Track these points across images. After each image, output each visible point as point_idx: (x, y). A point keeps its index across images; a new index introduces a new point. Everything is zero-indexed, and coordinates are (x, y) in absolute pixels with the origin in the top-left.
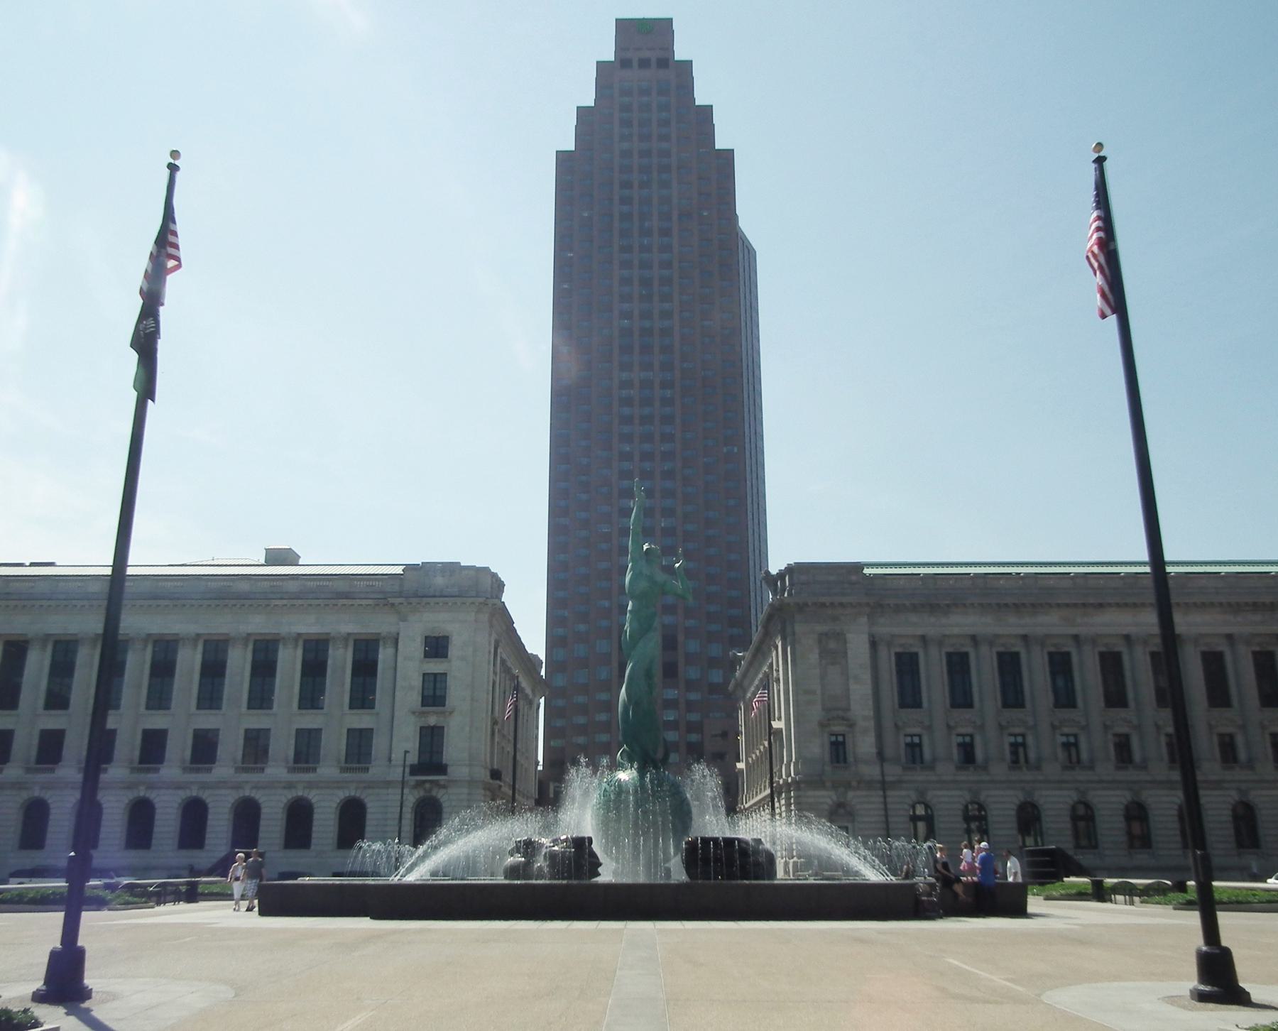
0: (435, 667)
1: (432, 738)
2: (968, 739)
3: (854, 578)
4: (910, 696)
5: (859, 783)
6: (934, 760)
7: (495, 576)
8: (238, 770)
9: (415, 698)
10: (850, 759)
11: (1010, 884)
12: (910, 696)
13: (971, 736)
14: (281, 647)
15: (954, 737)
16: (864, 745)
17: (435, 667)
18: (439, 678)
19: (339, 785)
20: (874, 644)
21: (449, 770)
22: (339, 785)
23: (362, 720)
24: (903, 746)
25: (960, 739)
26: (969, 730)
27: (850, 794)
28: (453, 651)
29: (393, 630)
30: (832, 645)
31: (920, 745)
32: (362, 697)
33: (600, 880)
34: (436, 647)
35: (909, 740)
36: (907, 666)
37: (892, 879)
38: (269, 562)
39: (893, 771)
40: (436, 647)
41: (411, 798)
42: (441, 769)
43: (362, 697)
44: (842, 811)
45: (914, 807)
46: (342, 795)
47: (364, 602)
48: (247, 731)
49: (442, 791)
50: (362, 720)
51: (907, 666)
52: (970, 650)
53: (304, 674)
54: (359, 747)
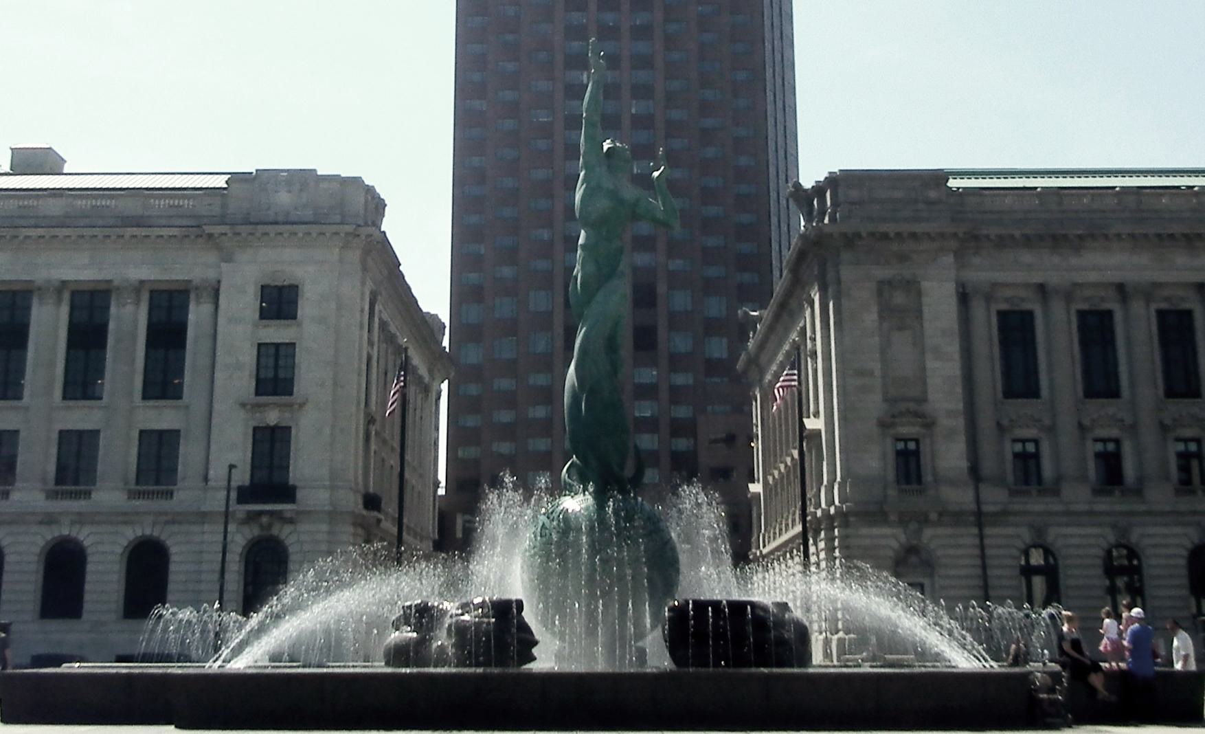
0: (276, 333)
1: (271, 445)
2: (1111, 447)
3: (933, 194)
4: (1020, 379)
5: (941, 514)
6: (1059, 479)
7: (370, 190)
8: (133, 495)
9: (244, 383)
10: (928, 478)
11: (1179, 672)
12: (1020, 379)
13: (1117, 442)
14: (192, 296)
15: (1089, 444)
16: (949, 456)
17: (276, 333)
18: (282, 351)
19: (126, 518)
20: (964, 298)
21: (300, 494)
22: (126, 518)
23: (162, 417)
24: (1009, 457)
25: (1099, 447)
26: (1114, 432)
27: (928, 533)
28: (306, 309)
29: (211, 275)
30: (899, 298)
31: (1036, 456)
32: (163, 381)
33: (535, 667)
34: (279, 302)
35: (1018, 447)
36: (1016, 331)
37: (993, 666)
38: (16, 170)
39: (994, 498)
40: (279, 302)
41: (240, 538)
42: (287, 493)
43: (163, 381)
44: (913, 559)
45: (1026, 554)
46: (130, 534)
47: (165, 232)
48: (61, 432)
49: (287, 529)
50: (162, 417)
51: (1016, 331)
52: (1116, 307)
53: (151, 343)
54: (158, 458)
